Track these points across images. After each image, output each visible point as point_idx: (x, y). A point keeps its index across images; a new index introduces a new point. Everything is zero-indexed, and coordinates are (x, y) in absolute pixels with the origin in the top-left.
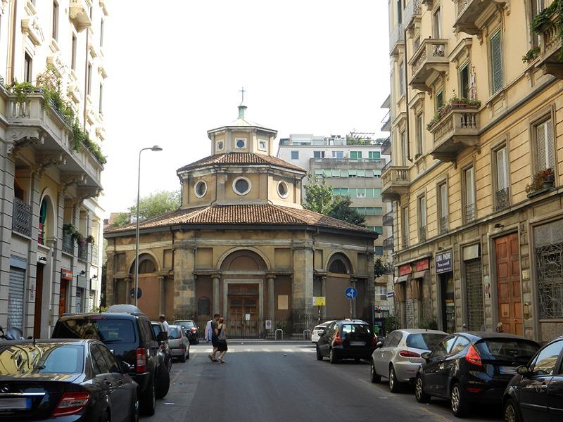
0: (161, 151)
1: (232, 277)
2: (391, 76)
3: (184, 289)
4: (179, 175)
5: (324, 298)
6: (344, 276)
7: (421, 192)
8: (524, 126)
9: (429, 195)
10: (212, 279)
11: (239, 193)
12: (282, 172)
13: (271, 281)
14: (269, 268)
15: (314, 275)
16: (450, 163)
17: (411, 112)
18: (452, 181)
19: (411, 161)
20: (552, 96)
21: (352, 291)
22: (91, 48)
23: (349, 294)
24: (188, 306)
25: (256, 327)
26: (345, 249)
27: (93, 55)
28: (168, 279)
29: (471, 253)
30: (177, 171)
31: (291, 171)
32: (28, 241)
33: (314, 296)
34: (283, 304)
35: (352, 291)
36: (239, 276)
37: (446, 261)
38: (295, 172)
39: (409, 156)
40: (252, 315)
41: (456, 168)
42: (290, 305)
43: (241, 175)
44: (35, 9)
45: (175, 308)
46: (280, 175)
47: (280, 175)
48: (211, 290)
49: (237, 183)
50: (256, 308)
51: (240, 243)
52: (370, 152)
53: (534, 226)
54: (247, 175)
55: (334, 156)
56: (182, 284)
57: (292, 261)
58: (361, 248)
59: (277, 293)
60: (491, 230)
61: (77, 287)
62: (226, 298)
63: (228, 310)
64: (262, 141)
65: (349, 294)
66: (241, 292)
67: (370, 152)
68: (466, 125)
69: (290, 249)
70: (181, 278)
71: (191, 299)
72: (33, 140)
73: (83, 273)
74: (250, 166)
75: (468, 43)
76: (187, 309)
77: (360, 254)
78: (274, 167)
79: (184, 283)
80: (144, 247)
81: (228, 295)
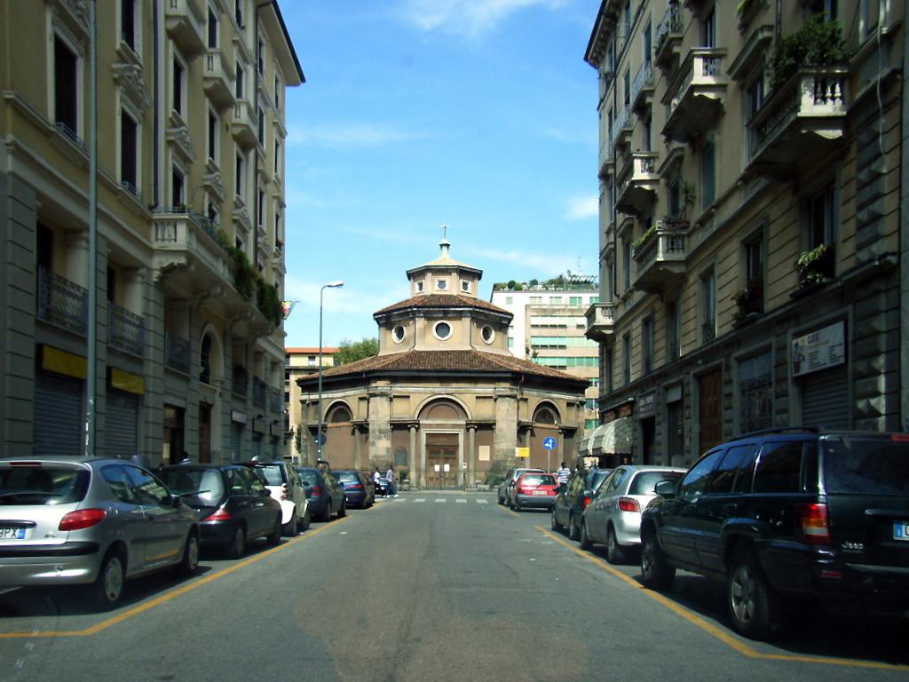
0: (343, 287)
1: (430, 426)
2: (600, 202)
3: (380, 438)
4: (376, 319)
5: (528, 449)
6: (551, 426)
7: (626, 330)
8: (735, 244)
9: (634, 334)
10: (409, 429)
11: (440, 338)
12: (486, 315)
13: (472, 430)
14: (470, 418)
15: (518, 425)
16: (656, 295)
17: (619, 240)
18: (657, 316)
19: (618, 296)
20: (766, 207)
21: (551, 441)
22: (263, 173)
23: (547, 445)
24: (385, 456)
25: (455, 479)
26: (552, 399)
27: (266, 181)
28: (363, 428)
29: (675, 396)
30: (374, 315)
31: (496, 314)
32: (188, 380)
33: (518, 446)
34: (484, 454)
35: (551, 441)
36: (438, 426)
37: (648, 405)
38: (501, 315)
39: (615, 292)
40: (451, 466)
41: (662, 300)
42: (491, 457)
43: (442, 318)
44: (265, 161)
45: (370, 458)
46: (484, 318)
47: (484, 318)
48: (408, 440)
49: (438, 326)
50: (456, 459)
51: (438, 390)
52: (591, 298)
53: (740, 360)
54: (449, 319)
55: (778, 412)
56: (377, 433)
57: (494, 410)
58: (572, 398)
59: (478, 443)
60: (700, 368)
61: (253, 431)
62: (423, 448)
63: (426, 461)
64: (465, 281)
65: (547, 445)
66: (442, 441)
67: (591, 298)
68: (673, 249)
69: (491, 397)
70: (376, 427)
71: (388, 449)
72: (181, 267)
73: (260, 417)
74: (452, 309)
75: (680, 153)
76: (383, 459)
77: (570, 404)
78: (501, 315)
79: (380, 433)
80: (337, 395)
81: (427, 445)
